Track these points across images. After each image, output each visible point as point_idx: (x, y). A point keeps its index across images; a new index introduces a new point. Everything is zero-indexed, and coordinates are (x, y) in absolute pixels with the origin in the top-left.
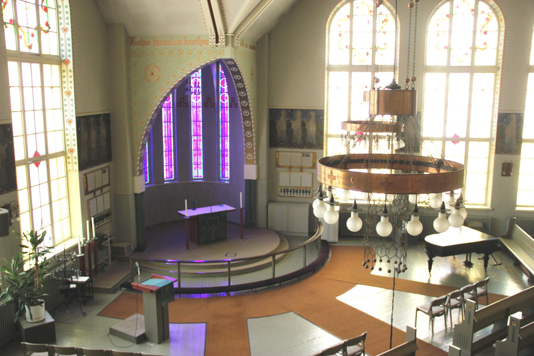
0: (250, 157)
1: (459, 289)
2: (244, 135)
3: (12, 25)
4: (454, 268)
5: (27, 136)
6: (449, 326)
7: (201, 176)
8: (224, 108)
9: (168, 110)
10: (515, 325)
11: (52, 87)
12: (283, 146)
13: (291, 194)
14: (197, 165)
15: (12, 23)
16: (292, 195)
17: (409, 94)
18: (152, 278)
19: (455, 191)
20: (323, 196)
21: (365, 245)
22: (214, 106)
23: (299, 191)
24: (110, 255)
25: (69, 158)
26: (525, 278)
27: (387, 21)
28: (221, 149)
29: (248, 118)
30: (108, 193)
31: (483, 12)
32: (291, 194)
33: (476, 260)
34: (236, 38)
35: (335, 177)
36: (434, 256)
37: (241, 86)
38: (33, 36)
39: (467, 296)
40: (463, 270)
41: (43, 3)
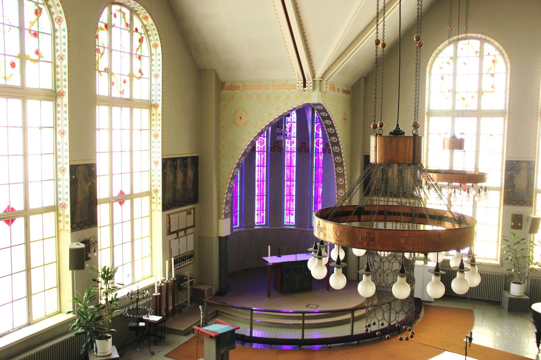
2: (336, 182)
3: (107, 73)
5: (113, 175)
7: (293, 223)
8: (318, 154)
9: (262, 154)
11: (141, 130)
14: (289, 211)
15: (107, 71)
18: (215, 323)
22: (308, 151)
24: (189, 297)
25: (154, 198)
27: (496, 62)
28: (314, 196)
29: (341, 164)
30: (193, 235)
34: (325, 82)
37: (333, 131)
38: (125, 82)
41: (138, 52)
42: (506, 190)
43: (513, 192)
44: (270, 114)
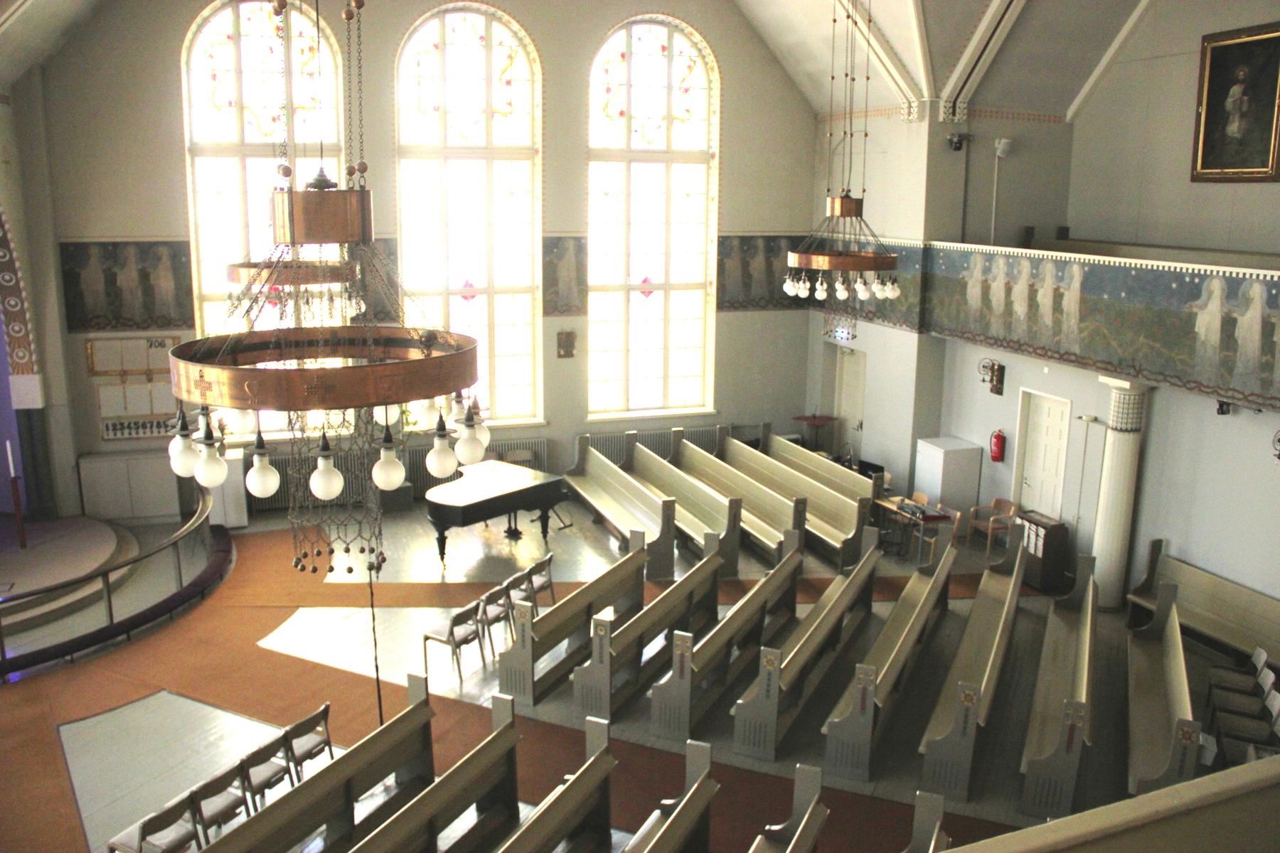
0: (22, 358)
1: (501, 584)
4: (488, 545)
6: (489, 658)
10: (602, 633)
12: (100, 328)
13: (130, 434)
16: (134, 435)
17: (354, 201)
19: (465, 392)
20: (190, 428)
21: (293, 523)
23: (148, 425)
26: (614, 544)
32: (130, 434)
33: (527, 523)
35: (210, 384)
36: (447, 528)
39: (516, 595)
40: (504, 546)
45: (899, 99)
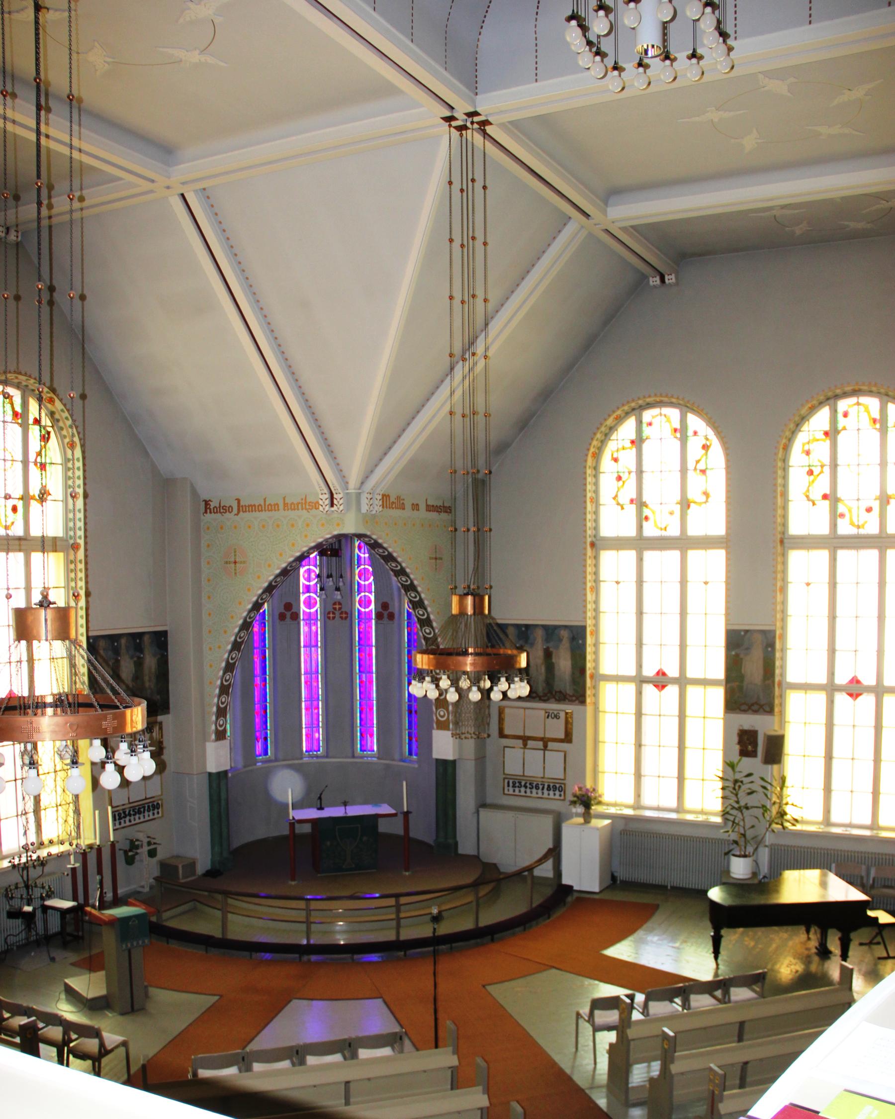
0: (442, 717)
16: (528, 794)
23: (541, 787)
31: (695, 433)
32: (526, 792)
42: (728, 686)
43: (741, 688)
44: (281, 555)
45: (317, 488)
